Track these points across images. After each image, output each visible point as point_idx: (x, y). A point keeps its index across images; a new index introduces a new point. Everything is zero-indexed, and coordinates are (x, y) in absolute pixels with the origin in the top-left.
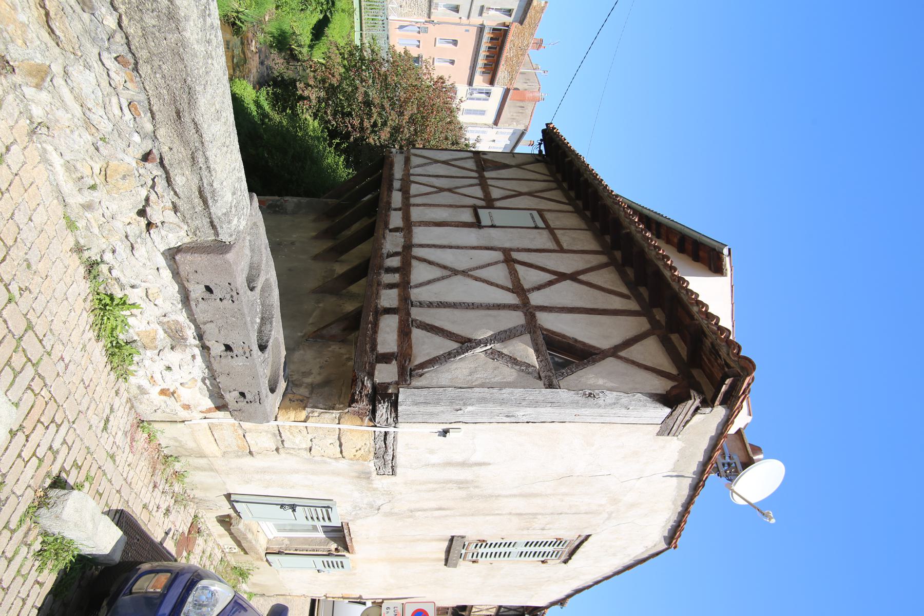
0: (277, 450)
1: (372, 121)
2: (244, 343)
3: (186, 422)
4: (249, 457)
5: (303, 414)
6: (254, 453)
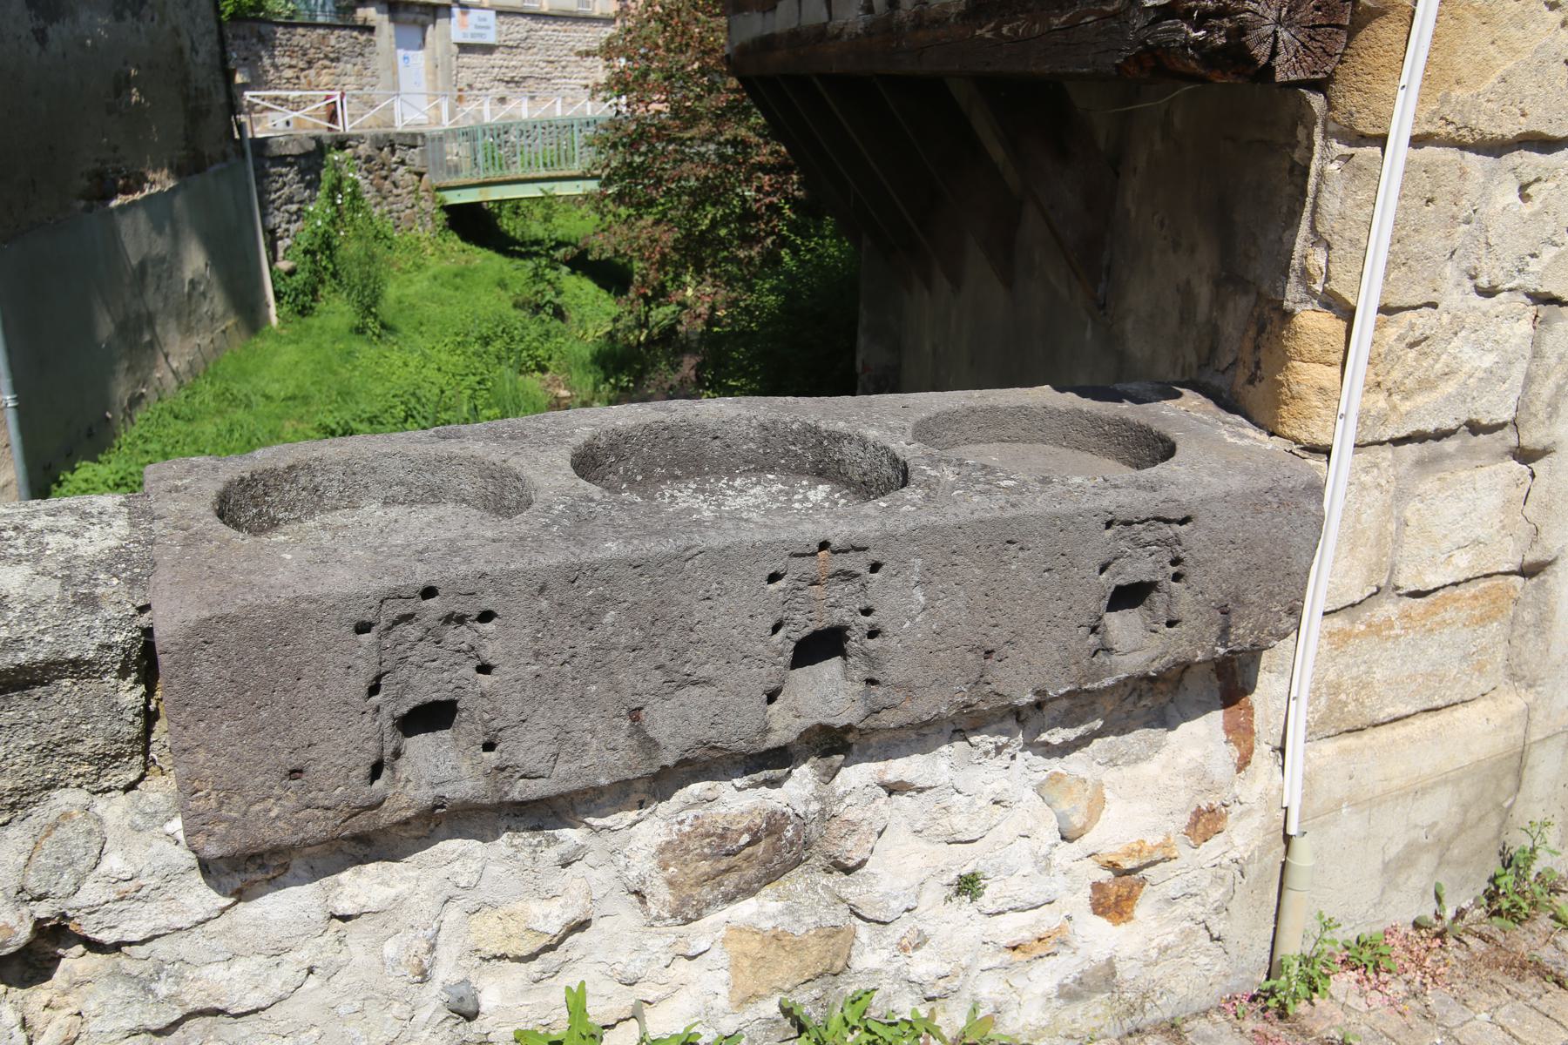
0: (1525, 456)
1: (754, 139)
2: (773, 578)
3: (1292, 830)
4: (1553, 578)
5: (1312, 321)
6: (1530, 558)
